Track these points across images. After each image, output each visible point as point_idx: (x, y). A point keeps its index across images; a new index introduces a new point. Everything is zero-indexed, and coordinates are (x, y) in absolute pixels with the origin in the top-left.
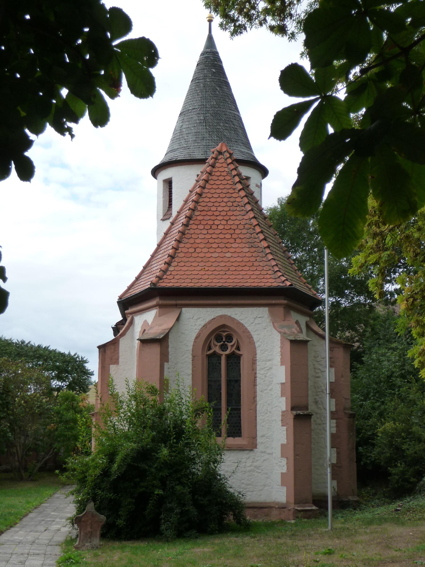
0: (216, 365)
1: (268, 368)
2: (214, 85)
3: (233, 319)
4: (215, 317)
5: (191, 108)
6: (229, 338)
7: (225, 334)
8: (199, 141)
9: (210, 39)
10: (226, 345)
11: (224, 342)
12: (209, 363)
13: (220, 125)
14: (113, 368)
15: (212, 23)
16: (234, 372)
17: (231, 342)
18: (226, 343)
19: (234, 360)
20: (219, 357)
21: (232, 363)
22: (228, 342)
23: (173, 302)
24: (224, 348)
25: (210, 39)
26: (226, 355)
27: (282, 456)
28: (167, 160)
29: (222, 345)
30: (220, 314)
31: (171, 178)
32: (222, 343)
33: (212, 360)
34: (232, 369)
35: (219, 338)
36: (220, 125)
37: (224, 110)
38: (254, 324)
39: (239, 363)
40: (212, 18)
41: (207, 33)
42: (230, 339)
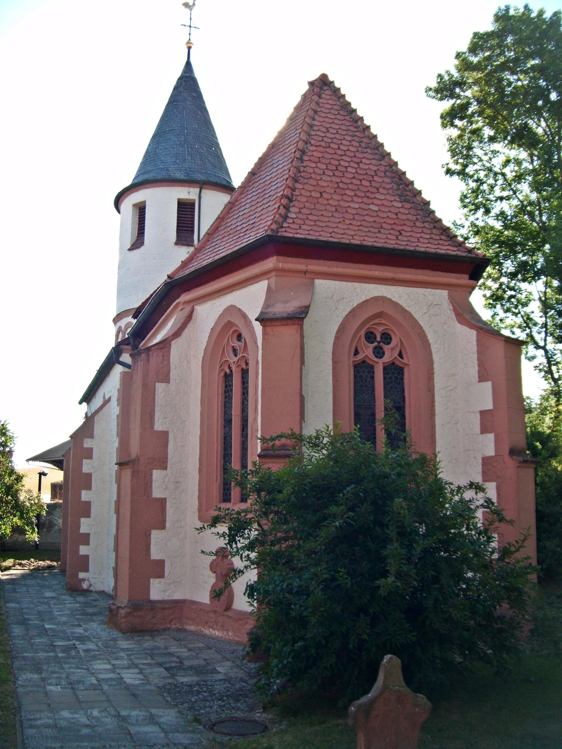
0: (366, 381)
1: (452, 388)
2: (195, 108)
3: (396, 305)
4: (368, 298)
5: (168, 129)
6: (387, 338)
7: (381, 329)
8: (180, 163)
9: (188, 64)
10: (381, 348)
11: (379, 343)
12: (355, 377)
13: (203, 149)
14: (160, 387)
15: (191, 50)
16: (394, 394)
17: (389, 343)
18: (382, 343)
19: (395, 373)
20: (371, 369)
21: (390, 378)
22: (385, 343)
23: (302, 267)
24: (379, 352)
25: (188, 64)
26: (383, 363)
27: (162, 502)
28: (140, 179)
29: (375, 348)
30: (376, 294)
31: (144, 202)
32: (376, 344)
33: (363, 371)
34: (391, 388)
35: (370, 336)
36: (203, 149)
37: (207, 135)
38: (427, 314)
39: (402, 379)
40: (191, 45)
41: (186, 59)
42: (386, 339)
